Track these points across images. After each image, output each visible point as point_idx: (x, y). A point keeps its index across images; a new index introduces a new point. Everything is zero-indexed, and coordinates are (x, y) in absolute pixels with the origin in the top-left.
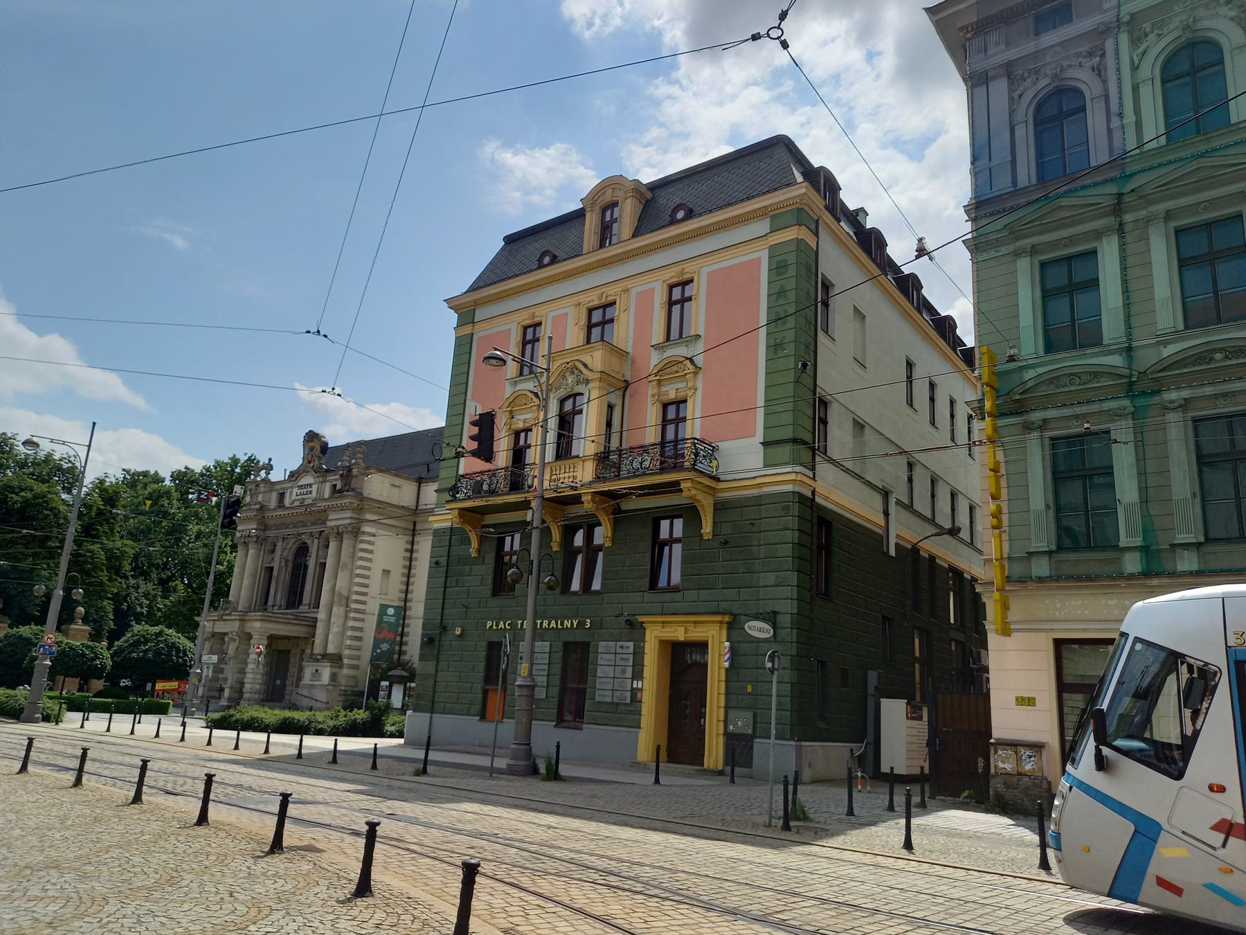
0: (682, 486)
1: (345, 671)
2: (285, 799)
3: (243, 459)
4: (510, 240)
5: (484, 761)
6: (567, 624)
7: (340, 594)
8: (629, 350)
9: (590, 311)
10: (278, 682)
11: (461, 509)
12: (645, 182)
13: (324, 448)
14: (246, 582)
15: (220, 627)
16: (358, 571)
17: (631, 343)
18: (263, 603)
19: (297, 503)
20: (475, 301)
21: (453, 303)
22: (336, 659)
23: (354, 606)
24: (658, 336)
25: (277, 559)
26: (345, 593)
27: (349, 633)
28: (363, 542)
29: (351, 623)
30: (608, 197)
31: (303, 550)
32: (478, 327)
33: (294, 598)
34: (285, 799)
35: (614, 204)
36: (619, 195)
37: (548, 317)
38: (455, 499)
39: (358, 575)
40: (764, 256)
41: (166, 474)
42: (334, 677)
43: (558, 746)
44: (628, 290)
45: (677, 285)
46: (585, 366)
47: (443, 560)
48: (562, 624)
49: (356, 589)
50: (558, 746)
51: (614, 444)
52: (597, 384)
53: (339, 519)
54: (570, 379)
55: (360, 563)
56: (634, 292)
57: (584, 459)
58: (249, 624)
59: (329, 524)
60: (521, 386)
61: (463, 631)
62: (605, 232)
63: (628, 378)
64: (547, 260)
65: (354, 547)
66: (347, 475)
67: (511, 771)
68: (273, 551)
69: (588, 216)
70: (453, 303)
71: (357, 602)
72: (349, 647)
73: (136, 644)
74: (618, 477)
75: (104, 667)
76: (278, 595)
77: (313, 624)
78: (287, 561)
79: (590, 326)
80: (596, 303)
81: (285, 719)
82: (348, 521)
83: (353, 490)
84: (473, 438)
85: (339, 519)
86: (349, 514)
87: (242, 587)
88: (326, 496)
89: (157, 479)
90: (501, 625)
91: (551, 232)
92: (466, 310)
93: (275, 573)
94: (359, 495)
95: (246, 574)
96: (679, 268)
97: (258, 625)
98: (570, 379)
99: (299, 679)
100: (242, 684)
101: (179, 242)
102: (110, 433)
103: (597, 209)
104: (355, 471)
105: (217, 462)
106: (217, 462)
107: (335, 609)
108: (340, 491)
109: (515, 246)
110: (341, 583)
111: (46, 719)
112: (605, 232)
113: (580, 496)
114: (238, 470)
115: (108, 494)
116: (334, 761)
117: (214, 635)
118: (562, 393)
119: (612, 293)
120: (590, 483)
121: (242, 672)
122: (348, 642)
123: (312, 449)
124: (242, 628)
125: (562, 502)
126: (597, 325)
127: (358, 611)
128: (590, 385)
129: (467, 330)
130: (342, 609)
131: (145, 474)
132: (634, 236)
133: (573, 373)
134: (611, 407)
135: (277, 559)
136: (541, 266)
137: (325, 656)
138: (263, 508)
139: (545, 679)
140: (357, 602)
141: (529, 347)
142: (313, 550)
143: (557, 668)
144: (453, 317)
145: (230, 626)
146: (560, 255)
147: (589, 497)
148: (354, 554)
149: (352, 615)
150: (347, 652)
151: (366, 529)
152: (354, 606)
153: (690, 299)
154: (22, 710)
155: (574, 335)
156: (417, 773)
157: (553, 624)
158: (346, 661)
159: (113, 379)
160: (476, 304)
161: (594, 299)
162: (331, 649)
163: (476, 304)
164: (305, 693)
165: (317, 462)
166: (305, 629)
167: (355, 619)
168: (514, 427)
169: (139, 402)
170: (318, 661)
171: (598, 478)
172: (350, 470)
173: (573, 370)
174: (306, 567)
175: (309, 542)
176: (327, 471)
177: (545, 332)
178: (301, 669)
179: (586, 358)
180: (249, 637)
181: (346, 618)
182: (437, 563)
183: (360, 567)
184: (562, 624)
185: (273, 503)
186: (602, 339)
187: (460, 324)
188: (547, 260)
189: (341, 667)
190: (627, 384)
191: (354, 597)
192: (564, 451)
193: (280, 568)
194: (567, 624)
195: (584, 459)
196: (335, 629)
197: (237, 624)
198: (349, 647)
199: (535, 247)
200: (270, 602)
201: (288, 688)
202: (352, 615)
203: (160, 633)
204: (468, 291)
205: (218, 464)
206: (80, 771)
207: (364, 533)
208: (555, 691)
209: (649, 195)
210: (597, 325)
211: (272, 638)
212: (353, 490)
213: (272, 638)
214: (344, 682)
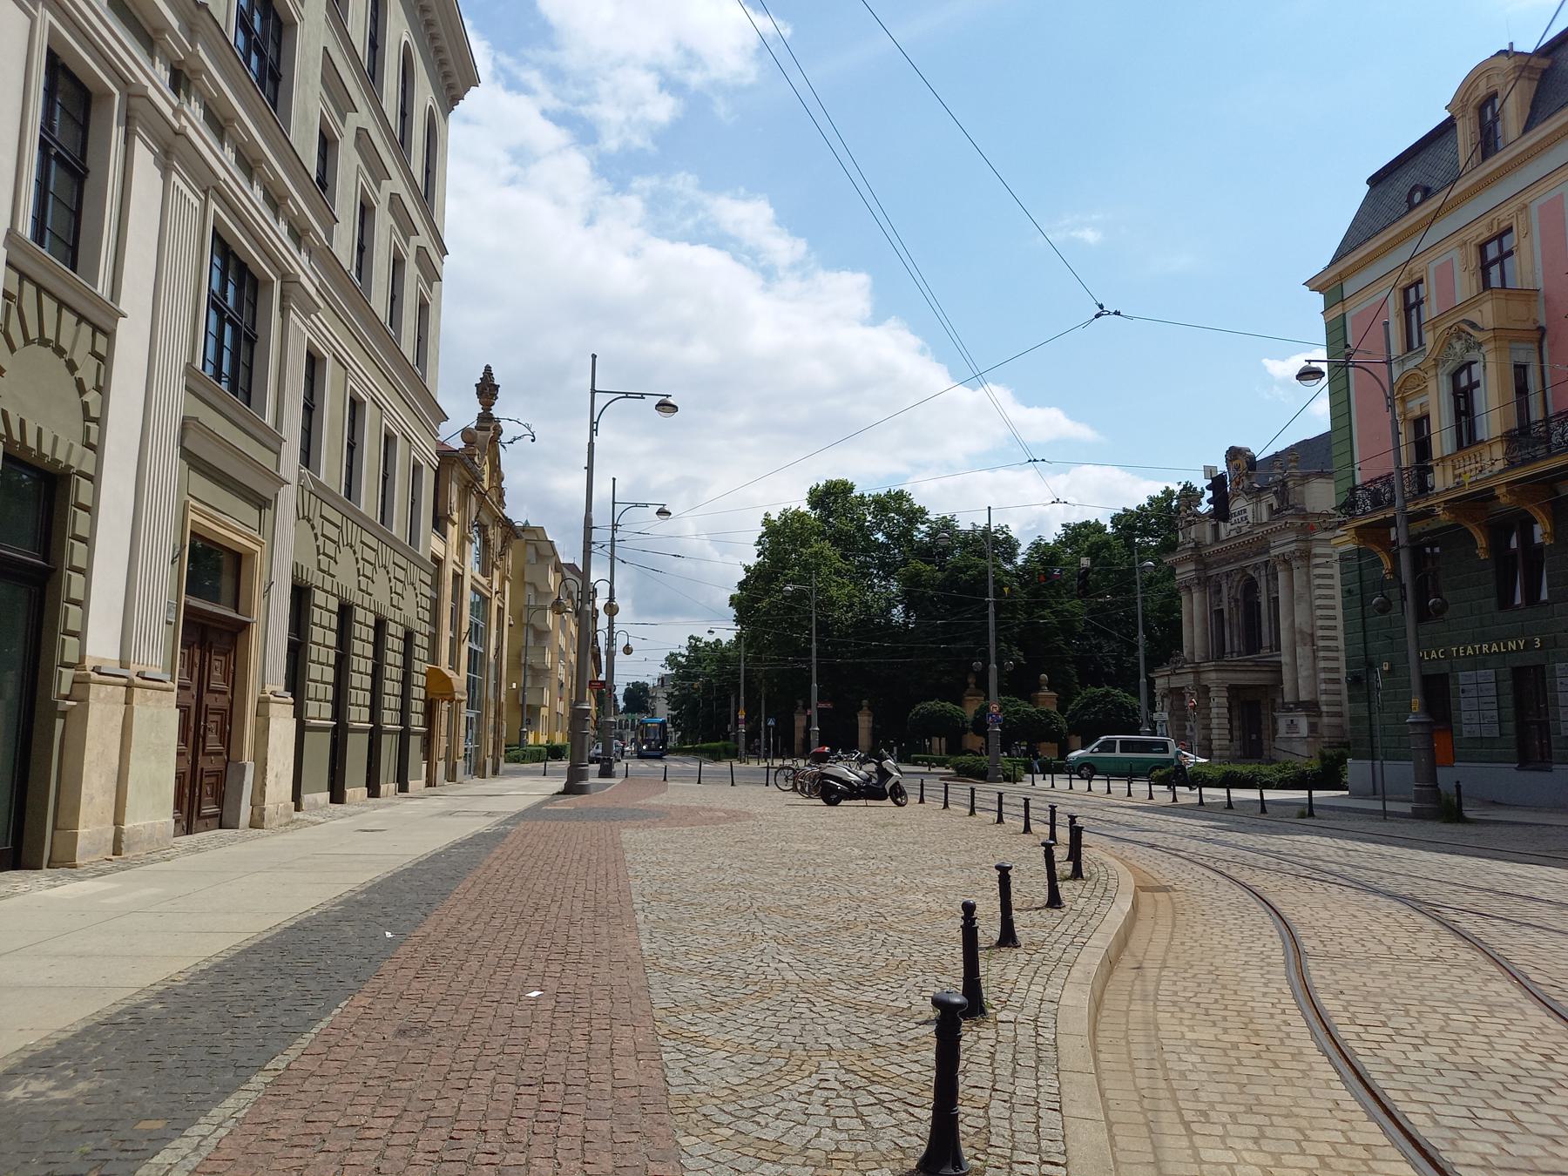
0: (1497, 492)
1: (1326, 720)
2: (1000, 795)
3: (1177, 489)
4: (1374, 181)
5: (1378, 806)
6: (1512, 645)
7: (1301, 632)
8: (1540, 285)
9: (1482, 248)
10: (1254, 737)
11: (1446, 502)
12: (1530, 49)
13: (1252, 463)
14: (1197, 630)
15: (1176, 682)
16: (1318, 602)
17: (1539, 276)
18: (1218, 652)
19: (1233, 534)
20: (1340, 274)
21: (1314, 284)
22: (1311, 707)
23: (1321, 643)
24: (1397, 349)
25: (1225, 600)
26: (1307, 630)
27: (1322, 676)
28: (1317, 566)
29: (1322, 664)
30: (1482, 91)
31: (1251, 586)
32: (1348, 304)
33: (1252, 641)
34: (1000, 795)
35: (1493, 96)
36: (1497, 82)
37: (1428, 267)
38: (1353, 516)
39: (1319, 607)
40: (1457, 255)
41: (1106, 522)
42: (1313, 728)
43: (1458, 786)
44: (1526, 206)
45: (1490, 241)
46: (1473, 325)
47: (1355, 587)
48: (1506, 646)
49: (1320, 623)
50: (1458, 786)
51: (1536, 414)
52: (1492, 345)
53: (1284, 545)
54: (1458, 346)
55: (1318, 592)
56: (1534, 210)
57: (1489, 444)
58: (1204, 676)
59: (1273, 552)
60: (1410, 365)
61: (1391, 666)
62: (1488, 143)
63: (1543, 323)
64: (1418, 197)
65: (1308, 574)
66: (1283, 492)
67: (1418, 815)
68: (1219, 591)
69: (1459, 124)
70: (1314, 284)
71: (1324, 638)
72: (1326, 692)
73: (1086, 707)
74: (1550, 455)
75: (1060, 729)
76: (1234, 640)
77: (1277, 668)
78: (1236, 601)
79: (1485, 268)
80: (1486, 235)
81: (1227, 773)
82: (1293, 547)
83: (1293, 507)
84: (1209, 501)
85: (1284, 545)
86: (1293, 536)
87: (1194, 636)
88: (1265, 519)
89: (1098, 528)
90: (1434, 655)
91: (1423, 156)
92: (1331, 286)
93: (1226, 615)
94: (1303, 514)
95: (1196, 621)
96: (1487, 221)
97: (1213, 675)
98: (1458, 346)
99: (1275, 731)
100: (1210, 740)
101: (1090, 236)
102: (1062, 476)
103: (1471, 112)
104: (1290, 484)
105: (1151, 498)
106: (1151, 498)
107: (1299, 650)
108: (1278, 511)
109: (1380, 188)
110: (1301, 618)
111: (1007, 779)
112: (1488, 143)
113: (1492, 489)
114: (1174, 503)
115: (1045, 555)
116: (1263, 810)
117: (1171, 691)
118: (1451, 366)
119: (1504, 216)
120: (1501, 472)
121: (1207, 727)
122: (1323, 686)
123: (1237, 467)
124: (1197, 680)
125: (1475, 503)
126: (1494, 262)
127: (1327, 649)
128: (1484, 349)
129: (1337, 311)
130: (1308, 648)
131: (1086, 524)
132: (1527, 129)
133: (1459, 338)
134: (1521, 370)
135: (1225, 600)
136: (1412, 207)
137: (1299, 704)
138: (1198, 545)
139: (1495, 713)
140: (1324, 638)
141: (1414, 312)
142: (1263, 584)
143: (1508, 700)
144: (1318, 299)
145: (1186, 680)
146: (1435, 185)
147: (1504, 490)
148: (1309, 581)
149: (1321, 654)
150: (1324, 698)
151: (1317, 550)
152: (1321, 643)
153: (1510, 253)
154: (986, 772)
155: (1465, 285)
156: (1302, 816)
157: (1495, 648)
158: (1324, 708)
159: (1054, 414)
160: (1342, 278)
161: (1482, 232)
162: (1304, 696)
163: (1342, 278)
164: (1284, 746)
165: (1246, 482)
166: (1269, 675)
167: (1326, 659)
168: (1409, 416)
169: (1084, 432)
170: (1290, 710)
171: (1512, 465)
172: (1285, 485)
173: (1459, 334)
174: (1259, 604)
175: (1256, 575)
176: (1260, 490)
177: (1429, 290)
178: (1275, 721)
179: (1473, 316)
180: (1207, 689)
181: (1315, 658)
182: (1349, 591)
183: (1320, 597)
184: (1506, 646)
185: (1209, 539)
186: (1504, 286)
187: (1328, 307)
188: (1418, 197)
189: (1320, 715)
190: (1542, 331)
191: (1320, 633)
192: (1466, 434)
193: (1230, 609)
194: (1512, 645)
195: (1489, 444)
196: (1303, 673)
197: (1191, 677)
198: (1326, 692)
199: (1402, 184)
200: (1228, 649)
201: (1265, 742)
202: (1321, 654)
203: (1107, 694)
204: (1332, 263)
205: (1152, 500)
206: (1000, 811)
207: (1316, 556)
208: (1510, 726)
209: (1545, 63)
210: (1494, 262)
211: (1234, 691)
212: (1293, 507)
213: (1234, 691)
214: (1326, 732)
